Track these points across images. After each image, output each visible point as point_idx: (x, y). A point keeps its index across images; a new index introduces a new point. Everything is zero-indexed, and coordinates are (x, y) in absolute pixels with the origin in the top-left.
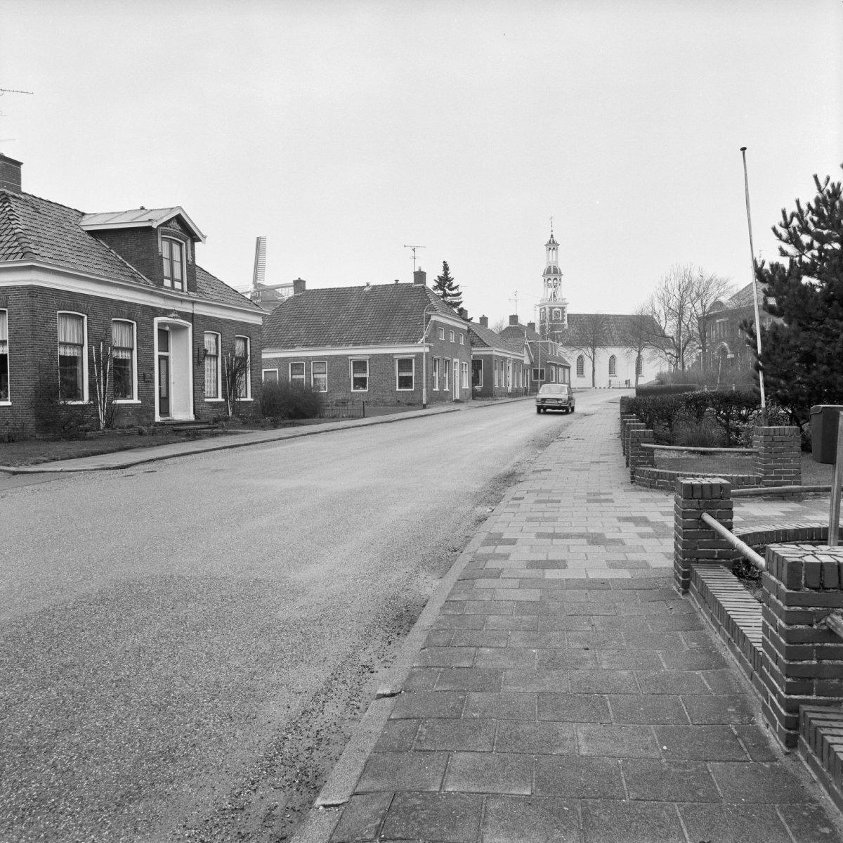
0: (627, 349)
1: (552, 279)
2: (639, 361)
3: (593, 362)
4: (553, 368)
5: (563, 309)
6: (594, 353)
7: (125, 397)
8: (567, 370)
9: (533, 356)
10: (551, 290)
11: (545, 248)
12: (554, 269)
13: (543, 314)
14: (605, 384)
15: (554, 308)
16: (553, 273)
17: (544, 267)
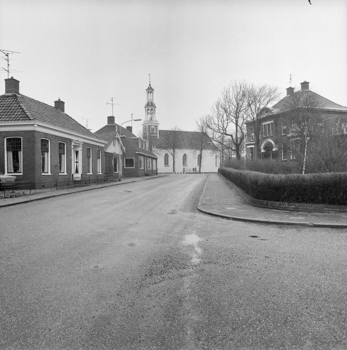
0: (194, 150)
1: (150, 110)
2: (200, 157)
3: (174, 157)
4: (142, 158)
5: (156, 126)
6: (174, 151)
7: (16, 171)
8: (154, 161)
9: (124, 148)
10: (149, 116)
11: (146, 92)
12: (151, 103)
13: (145, 129)
14: (181, 170)
15: (152, 126)
16: (150, 106)
17: (146, 102)
